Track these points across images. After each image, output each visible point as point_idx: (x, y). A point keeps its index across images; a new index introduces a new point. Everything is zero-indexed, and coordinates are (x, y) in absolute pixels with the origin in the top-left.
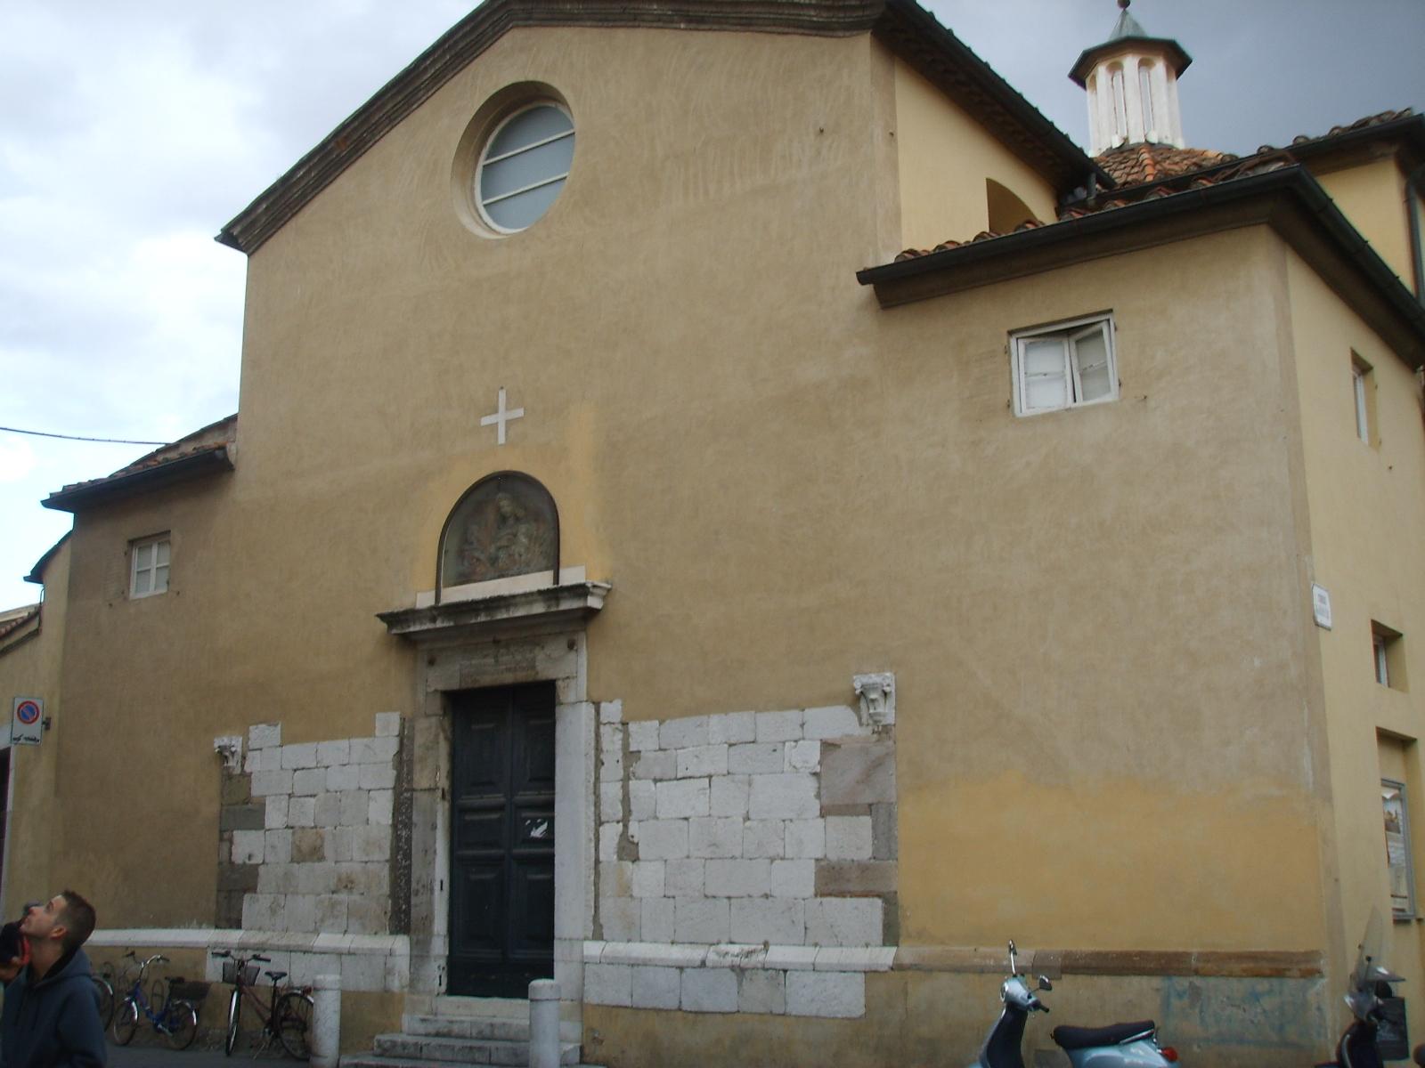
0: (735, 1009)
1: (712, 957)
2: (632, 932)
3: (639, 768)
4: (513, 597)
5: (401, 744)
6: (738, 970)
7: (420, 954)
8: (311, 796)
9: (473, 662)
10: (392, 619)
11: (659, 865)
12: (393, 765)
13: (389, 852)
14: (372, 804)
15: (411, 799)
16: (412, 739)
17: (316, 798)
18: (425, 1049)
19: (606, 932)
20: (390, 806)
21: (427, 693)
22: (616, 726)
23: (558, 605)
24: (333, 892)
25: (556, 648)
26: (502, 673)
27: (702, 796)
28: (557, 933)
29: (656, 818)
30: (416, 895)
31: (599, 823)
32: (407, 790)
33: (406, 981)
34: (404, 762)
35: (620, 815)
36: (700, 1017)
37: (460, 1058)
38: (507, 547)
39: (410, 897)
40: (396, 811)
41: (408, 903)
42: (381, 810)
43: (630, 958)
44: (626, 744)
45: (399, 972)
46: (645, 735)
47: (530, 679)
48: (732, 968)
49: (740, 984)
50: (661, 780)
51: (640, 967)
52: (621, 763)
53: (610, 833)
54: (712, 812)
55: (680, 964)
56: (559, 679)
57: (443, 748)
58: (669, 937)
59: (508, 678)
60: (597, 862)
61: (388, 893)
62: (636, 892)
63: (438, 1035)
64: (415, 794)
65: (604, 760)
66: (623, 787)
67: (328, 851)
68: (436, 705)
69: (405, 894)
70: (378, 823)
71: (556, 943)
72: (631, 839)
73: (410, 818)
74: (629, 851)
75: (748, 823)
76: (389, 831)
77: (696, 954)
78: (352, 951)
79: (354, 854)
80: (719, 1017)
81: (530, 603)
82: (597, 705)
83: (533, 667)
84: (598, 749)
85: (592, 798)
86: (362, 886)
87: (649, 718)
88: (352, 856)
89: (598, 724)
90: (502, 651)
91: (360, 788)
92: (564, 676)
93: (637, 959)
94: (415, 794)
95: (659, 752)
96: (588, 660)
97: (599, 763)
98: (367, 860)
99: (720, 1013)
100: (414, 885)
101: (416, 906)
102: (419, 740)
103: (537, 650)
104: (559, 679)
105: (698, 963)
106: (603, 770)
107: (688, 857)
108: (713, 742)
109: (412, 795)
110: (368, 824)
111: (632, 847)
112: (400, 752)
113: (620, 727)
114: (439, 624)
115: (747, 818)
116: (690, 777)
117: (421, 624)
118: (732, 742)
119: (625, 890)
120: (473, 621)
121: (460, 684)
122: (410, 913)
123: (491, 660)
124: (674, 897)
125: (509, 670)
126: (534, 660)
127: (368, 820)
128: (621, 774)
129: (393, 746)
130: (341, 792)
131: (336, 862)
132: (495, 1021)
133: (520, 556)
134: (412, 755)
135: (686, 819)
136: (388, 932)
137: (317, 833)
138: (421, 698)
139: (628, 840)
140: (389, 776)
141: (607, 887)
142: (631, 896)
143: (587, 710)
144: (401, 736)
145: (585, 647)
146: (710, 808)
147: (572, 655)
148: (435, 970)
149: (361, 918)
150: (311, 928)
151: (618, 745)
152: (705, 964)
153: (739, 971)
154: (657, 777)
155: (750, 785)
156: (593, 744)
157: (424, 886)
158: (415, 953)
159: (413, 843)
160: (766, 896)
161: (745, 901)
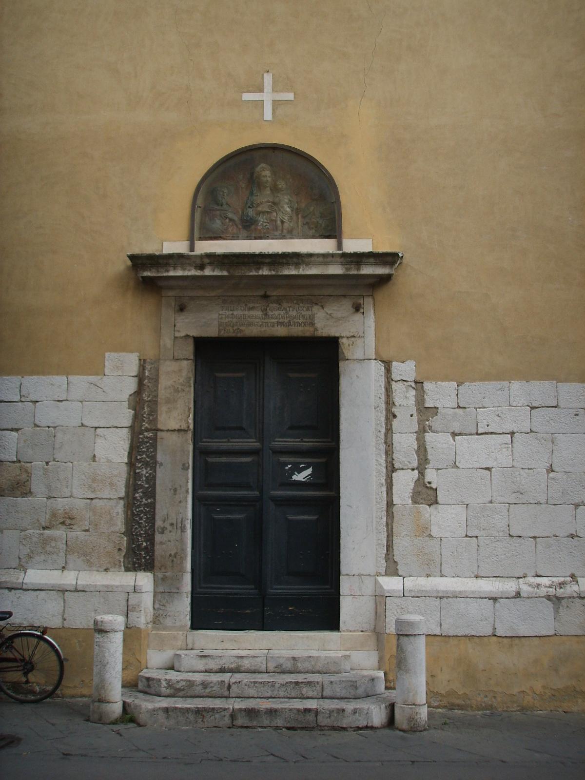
0: (552, 632)
1: (525, 589)
2: (432, 566)
3: (435, 422)
4: (311, 255)
5: (140, 383)
6: (554, 599)
7: (164, 593)
8: (12, 430)
9: (235, 313)
10: (138, 262)
11: (461, 509)
12: (129, 404)
13: (124, 489)
14: (99, 441)
15: (155, 439)
16: (156, 380)
17: (20, 432)
18: (234, 687)
19: (401, 569)
20: (126, 445)
21: (175, 338)
22: (410, 383)
23: (358, 269)
24: (44, 528)
25: (342, 309)
26: (273, 326)
27: (504, 450)
28: (344, 569)
29: (455, 466)
30: (162, 533)
31: (391, 468)
32: (147, 430)
33: (150, 618)
34: (143, 401)
35: (415, 464)
36: (517, 641)
37: (282, 694)
38: (268, 212)
39: (153, 535)
40: (134, 449)
41: (151, 538)
42: (114, 449)
43: (438, 591)
44: (420, 401)
45: (145, 609)
46: (440, 394)
47: (308, 334)
48: (548, 598)
49: (557, 611)
50: (460, 434)
51: (450, 599)
52: (415, 418)
53: (405, 481)
54: (515, 464)
55: (494, 596)
56: (342, 337)
57: (189, 396)
58: (473, 573)
59: (281, 331)
60: (390, 504)
61: (123, 530)
62: (435, 531)
63: (222, 670)
64: (159, 434)
65: (396, 413)
66: (417, 439)
67: (37, 485)
68: (189, 350)
69: (146, 533)
70: (109, 461)
71: (342, 579)
72: (428, 485)
73: (154, 457)
74: (426, 494)
75: (552, 475)
76: (124, 469)
77: (510, 586)
78: (79, 588)
79: (74, 490)
80: (536, 641)
81: (326, 264)
82: (387, 365)
83: (312, 324)
84: (389, 402)
85: (383, 447)
86: (87, 523)
87: (446, 378)
88: (71, 492)
89: (389, 380)
90: (271, 305)
91: (83, 425)
92: (349, 335)
93: (446, 592)
94: (159, 434)
95: (457, 410)
96: (376, 322)
97: (390, 416)
98: (92, 496)
99: (466, 636)
100: (159, 523)
101: (161, 543)
102: (165, 382)
103: (315, 309)
104: (342, 337)
105: (513, 594)
106: (395, 423)
107: (491, 502)
108: (514, 404)
109: (156, 435)
110: (94, 461)
111: (431, 492)
112: (138, 393)
113: (413, 385)
114: (208, 272)
115: (551, 470)
116: (492, 433)
117: (184, 269)
118: (535, 405)
119: (424, 530)
120: (254, 273)
121: (219, 331)
122: (153, 551)
123: (259, 313)
124: (476, 537)
125: (281, 324)
126: (312, 317)
127: (94, 456)
128: (416, 428)
129: (131, 386)
130: (55, 427)
131: (49, 498)
132: (296, 654)
133: (282, 222)
134: (156, 396)
135: (488, 469)
136: (123, 568)
137: (21, 468)
138: (167, 341)
139: (427, 487)
140: (126, 416)
141: (402, 528)
142: (430, 536)
143: (376, 369)
144: (140, 379)
145: (372, 311)
146: (513, 460)
147: (358, 317)
148: (183, 606)
149: (84, 555)
150: (15, 563)
151: (412, 401)
152: (520, 595)
153: (556, 600)
154: (457, 431)
155: (553, 442)
156: (383, 398)
157: (172, 524)
158: (161, 589)
159: (158, 482)
160: (572, 536)
161: (551, 541)
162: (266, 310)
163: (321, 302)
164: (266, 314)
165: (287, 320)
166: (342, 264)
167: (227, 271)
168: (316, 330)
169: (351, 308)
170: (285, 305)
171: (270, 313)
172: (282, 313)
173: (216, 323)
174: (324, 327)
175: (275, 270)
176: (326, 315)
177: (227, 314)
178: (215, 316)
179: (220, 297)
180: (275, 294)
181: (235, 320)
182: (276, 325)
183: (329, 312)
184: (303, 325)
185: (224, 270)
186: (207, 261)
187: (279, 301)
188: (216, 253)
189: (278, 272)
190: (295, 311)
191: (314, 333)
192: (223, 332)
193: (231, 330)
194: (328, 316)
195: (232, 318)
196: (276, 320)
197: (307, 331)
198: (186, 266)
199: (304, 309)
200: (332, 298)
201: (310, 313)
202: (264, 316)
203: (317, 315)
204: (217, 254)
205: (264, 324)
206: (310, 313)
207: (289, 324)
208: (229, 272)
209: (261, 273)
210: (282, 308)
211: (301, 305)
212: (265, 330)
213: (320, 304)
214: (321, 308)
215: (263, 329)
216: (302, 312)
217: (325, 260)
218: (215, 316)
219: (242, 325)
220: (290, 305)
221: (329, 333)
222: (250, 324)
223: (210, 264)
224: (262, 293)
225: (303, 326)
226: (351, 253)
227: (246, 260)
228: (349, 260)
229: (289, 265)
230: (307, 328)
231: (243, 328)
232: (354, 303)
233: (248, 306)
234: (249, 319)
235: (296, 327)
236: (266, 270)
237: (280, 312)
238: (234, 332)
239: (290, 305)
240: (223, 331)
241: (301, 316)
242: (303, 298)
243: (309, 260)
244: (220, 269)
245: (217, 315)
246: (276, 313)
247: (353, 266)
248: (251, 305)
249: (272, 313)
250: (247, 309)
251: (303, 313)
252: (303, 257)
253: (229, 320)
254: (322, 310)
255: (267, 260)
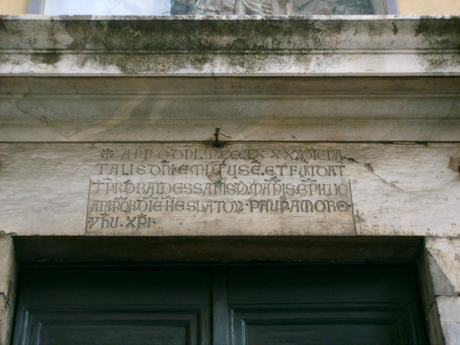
9: (135, 179)
47: (337, 230)
56: (434, 238)
59: (261, 224)
83: (347, 206)
90: (231, 162)
103: (351, 172)
114: (67, 66)
121: (90, 221)
123: (202, 181)
162: (220, 172)
163: (364, 157)
164: (219, 183)
165: (277, 197)
166: (422, 52)
167: (118, 65)
168: (358, 218)
169: (445, 169)
170: (268, 161)
171: (229, 180)
172: (261, 180)
173: (82, 202)
174: (380, 212)
175: (246, 65)
176: (382, 184)
177: (114, 181)
178: (79, 186)
179: (96, 145)
180: (240, 137)
181: (133, 196)
182: (247, 209)
183: (389, 179)
184: (320, 207)
185: (111, 63)
186: (65, 39)
187: (253, 152)
188: (91, 16)
189: (251, 68)
190: (297, 176)
191: (355, 229)
192: (98, 224)
193: (123, 220)
194: (389, 188)
195: (126, 190)
196: (248, 197)
197: (337, 224)
198: (9, 54)
199: (322, 171)
200: (392, 147)
201: (337, 180)
202: (213, 187)
203: (359, 185)
204: (93, 18)
205: (215, 206)
206: (337, 180)
207: (283, 205)
208: (123, 68)
209: (207, 69)
210: (262, 169)
211: (312, 162)
212: (216, 221)
213: (361, 160)
214: (365, 169)
215: (213, 217)
216: (316, 177)
217: (376, 39)
218: (82, 186)
219: (153, 207)
220: (282, 162)
221: (397, 228)
222: (174, 206)
223: (74, 48)
224: (208, 135)
225: (323, 211)
226: (443, 19)
227: (169, 37)
228: (439, 39)
229: (282, 55)
230: (333, 215)
231: (152, 215)
232: (452, 160)
233: (170, 164)
234: (172, 195)
235: (301, 214)
236: (222, 64)
237: (256, 177)
238: (131, 223)
239: (282, 162)
240: (100, 221)
241: (313, 188)
242: (315, 147)
243: (334, 39)
244: (101, 62)
245: (87, 183)
246: (244, 179)
247: (446, 57)
248: (179, 163)
249: (237, 181)
250: (166, 172)
251: (320, 181)
252: (319, 30)
253: (118, 195)
254: (369, 174)
255: (226, 40)
